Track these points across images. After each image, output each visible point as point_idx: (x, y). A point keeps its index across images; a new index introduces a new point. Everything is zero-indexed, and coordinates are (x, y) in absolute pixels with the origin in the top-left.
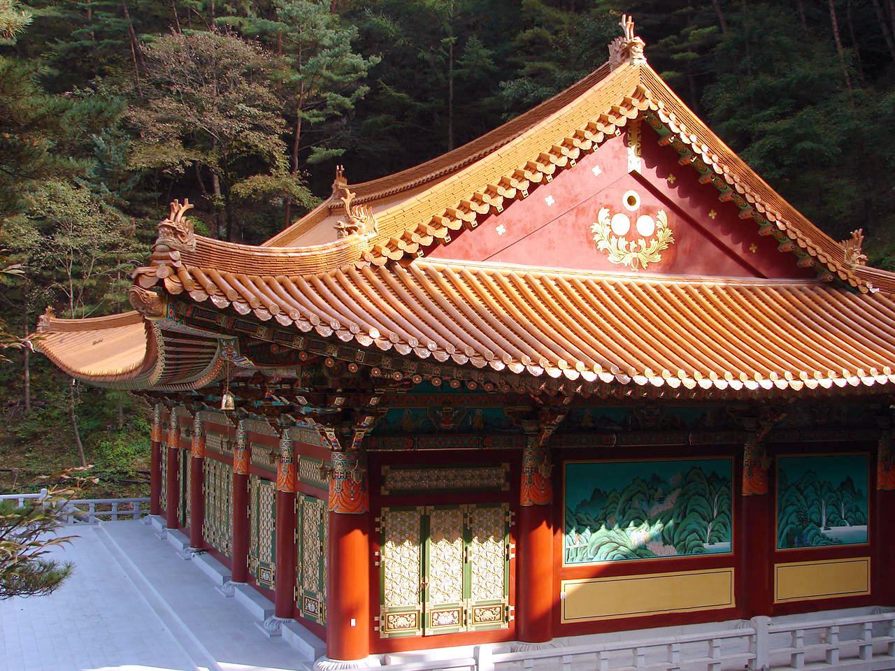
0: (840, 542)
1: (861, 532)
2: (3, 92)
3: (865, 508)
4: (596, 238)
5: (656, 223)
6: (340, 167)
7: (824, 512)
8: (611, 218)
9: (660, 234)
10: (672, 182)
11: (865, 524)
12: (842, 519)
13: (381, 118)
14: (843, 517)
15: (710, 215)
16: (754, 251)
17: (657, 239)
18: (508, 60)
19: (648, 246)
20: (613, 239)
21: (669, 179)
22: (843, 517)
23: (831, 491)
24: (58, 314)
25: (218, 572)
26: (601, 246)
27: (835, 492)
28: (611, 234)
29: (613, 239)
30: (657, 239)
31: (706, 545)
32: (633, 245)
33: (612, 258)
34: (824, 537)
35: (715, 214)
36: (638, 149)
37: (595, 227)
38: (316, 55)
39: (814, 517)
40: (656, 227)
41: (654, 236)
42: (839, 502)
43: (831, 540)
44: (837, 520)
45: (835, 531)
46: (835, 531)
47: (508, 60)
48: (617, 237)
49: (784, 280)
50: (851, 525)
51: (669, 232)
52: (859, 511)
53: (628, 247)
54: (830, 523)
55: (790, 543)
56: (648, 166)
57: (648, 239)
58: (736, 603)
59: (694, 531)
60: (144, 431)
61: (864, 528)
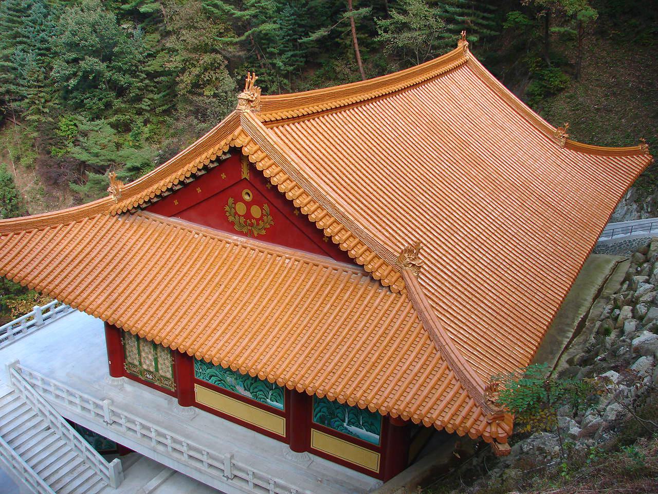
0: (358, 436)
4: (228, 214)
5: (262, 211)
7: (347, 415)
8: (235, 204)
9: (265, 218)
13: (217, 11)
17: (263, 221)
18: (496, 8)
19: (258, 224)
20: (237, 217)
24: (241, 7)
26: (231, 219)
28: (236, 213)
29: (237, 217)
30: (263, 221)
31: (268, 401)
32: (248, 221)
33: (236, 227)
34: (346, 429)
38: (542, 363)
39: (339, 415)
41: (261, 218)
43: (352, 433)
45: (353, 429)
46: (353, 429)
47: (496, 8)
48: (239, 216)
51: (270, 218)
52: (373, 425)
53: (245, 222)
55: (322, 419)
57: (258, 220)
59: (261, 391)
60: (559, 7)
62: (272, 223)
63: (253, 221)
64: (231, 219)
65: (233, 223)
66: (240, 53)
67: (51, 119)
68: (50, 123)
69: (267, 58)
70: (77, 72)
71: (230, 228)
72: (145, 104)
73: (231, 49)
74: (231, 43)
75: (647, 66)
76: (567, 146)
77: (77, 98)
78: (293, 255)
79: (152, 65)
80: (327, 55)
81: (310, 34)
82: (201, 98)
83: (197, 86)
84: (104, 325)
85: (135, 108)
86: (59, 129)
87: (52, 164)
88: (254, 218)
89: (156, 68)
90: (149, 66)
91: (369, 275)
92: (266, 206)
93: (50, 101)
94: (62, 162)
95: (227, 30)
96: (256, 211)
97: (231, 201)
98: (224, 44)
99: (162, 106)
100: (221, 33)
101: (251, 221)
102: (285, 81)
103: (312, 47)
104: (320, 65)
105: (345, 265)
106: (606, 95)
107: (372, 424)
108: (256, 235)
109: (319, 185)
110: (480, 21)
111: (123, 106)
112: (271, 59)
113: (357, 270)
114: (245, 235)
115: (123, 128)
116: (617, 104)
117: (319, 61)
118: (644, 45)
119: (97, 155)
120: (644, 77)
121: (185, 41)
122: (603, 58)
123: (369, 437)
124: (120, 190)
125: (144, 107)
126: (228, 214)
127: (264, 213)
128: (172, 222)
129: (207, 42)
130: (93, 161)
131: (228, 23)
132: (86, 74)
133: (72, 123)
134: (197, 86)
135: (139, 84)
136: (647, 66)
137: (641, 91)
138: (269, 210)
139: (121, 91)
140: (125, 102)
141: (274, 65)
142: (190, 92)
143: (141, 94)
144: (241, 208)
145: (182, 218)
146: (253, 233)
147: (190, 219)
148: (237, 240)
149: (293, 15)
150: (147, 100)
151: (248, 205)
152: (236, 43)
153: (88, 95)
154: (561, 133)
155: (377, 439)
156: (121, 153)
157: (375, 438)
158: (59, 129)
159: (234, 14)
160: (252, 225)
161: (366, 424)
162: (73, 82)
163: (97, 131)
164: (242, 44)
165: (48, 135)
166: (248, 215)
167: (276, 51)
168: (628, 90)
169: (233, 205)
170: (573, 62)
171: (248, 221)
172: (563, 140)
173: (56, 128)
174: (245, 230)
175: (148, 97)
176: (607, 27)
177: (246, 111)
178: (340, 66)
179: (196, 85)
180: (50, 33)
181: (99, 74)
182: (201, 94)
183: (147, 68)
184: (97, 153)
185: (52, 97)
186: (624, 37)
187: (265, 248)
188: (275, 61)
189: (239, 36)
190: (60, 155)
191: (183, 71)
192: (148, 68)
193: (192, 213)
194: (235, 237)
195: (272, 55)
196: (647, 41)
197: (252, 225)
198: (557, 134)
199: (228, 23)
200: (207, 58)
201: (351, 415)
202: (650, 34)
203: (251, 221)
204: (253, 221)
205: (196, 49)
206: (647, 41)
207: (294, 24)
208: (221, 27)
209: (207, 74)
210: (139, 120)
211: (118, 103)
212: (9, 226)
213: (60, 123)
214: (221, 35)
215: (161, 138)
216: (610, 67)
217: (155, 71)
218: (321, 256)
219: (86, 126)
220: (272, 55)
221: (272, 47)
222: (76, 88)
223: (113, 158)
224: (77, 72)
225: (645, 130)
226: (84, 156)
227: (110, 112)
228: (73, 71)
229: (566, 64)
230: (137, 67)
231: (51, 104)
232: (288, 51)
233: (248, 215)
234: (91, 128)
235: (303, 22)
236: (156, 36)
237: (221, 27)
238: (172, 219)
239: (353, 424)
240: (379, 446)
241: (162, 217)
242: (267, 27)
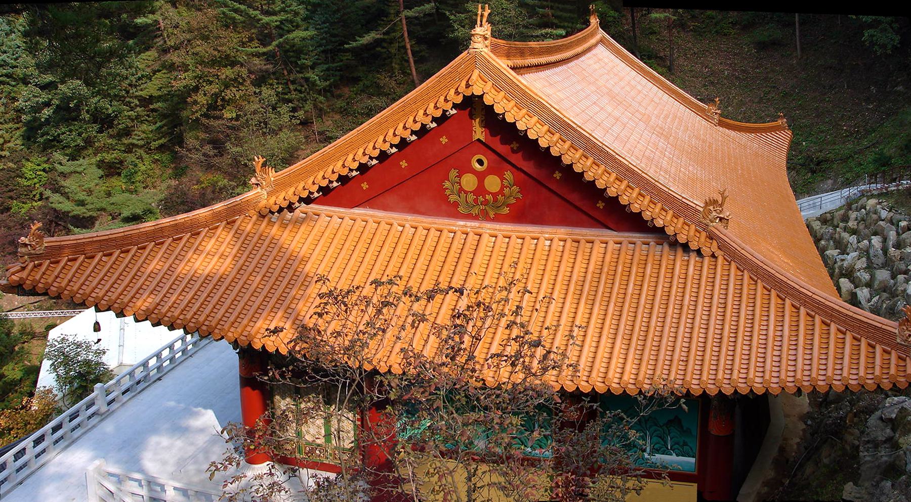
1: (688, 462)
2: (2, 150)
3: (695, 445)
4: (448, 192)
5: (502, 181)
6: (483, 8)
8: (460, 176)
9: (506, 191)
10: (515, 148)
11: (693, 457)
12: (668, 448)
14: (669, 448)
15: (555, 176)
16: (601, 207)
17: (503, 195)
20: (463, 195)
21: (512, 146)
22: (669, 448)
23: (657, 426)
25: (240, 375)
26: (453, 198)
27: (661, 427)
28: (461, 190)
29: (463, 195)
32: (481, 198)
33: (461, 209)
35: (560, 175)
36: (482, 121)
37: (447, 184)
40: (502, 185)
41: (501, 192)
42: (665, 435)
44: (662, 449)
45: (659, 457)
48: (466, 192)
49: (634, 235)
50: (677, 455)
51: (515, 189)
52: (687, 445)
53: (476, 201)
54: (655, 451)
56: (492, 135)
57: (495, 195)
58: (694, 483)
61: (693, 460)
62: (520, 196)
63: (488, 197)
64: (453, 198)
65: (456, 204)
66: (268, 66)
67: (11, 164)
68: (10, 170)
69: (298, 72)
70: (51, 100)
71: (452, 211)
72: (137, 138)
73: (256, 61)
74: (258, 55)
75: (735, 54)
76: (721, 124)
77: (48, 134)
78: (555, 233)
79: (145, 89)
80: (365, 68)
81: (358, 38)
82: (220, 122)
83: (215, 106)
84: (239, 383)
85: (125, 144)
86: (22, 176)
87: (12, 224)
88: (489, 193)
89: (152, 91)
90: (141, 90)
91: (674, 244)
92: (508, 175)
93: (9, 141)
94: (26, 220)
95: (251, 40)
96: (493, 183)
97: (453, 173)
98: (247, 55)
99: (160, 139)
100: (243, 43)
101: (484, 197)
102: (321, 98)
103: (347, 59)
104: (356, 80)
105: (630, 234)
106: (705, 85)
107: (685, 444)
108: (492, 216)
109: (591, 135)
110: (559, 13)
111: (110, 141)
112: (302, 73)
113: (647, 238)
114: (475, 218)
115: (111, 169)
116: (718, 93)
117: (355, 75)
118: (725, 35)
119: (82, 203)
120: (735, 64)
121: (197, 54)
122: (690, 49)
123: (679, 463)
124: (272, 179)
125: (135, 142)
126: (448, 192)
127: (506, 184)
128: (359, 214)
129: (228, 52)
130: (79, 211)
131: (252, 31)
132: (66, 99)
133: (39, 168)
134: (215, 106)
135: (131, 112)
136: (735, 54)
137: (737, 78)
138: (512, 177)
139: (104, 121)
140: (111, 137)
141: (307, 80)
142: (206, 116)
143: (132, 127)
144: (469, 182)
145: (372, 207)
146: (487, 213)
147: (385, 208)
148: (463, 226)
149: (324, 23)
150: (140, 133)
151: (481, 176)
152: (264, 54)
153: (63, 130)
154: (713, 109)
155: (692, 463)
156: (113, 200)
157: (688, 462)
158: (22, 176)
159: (261, 20)
160: (486, 203)
161: (676, 446)
162: (47, 112)
163: (80, 173)
164: (269, 57)
165: (7, 186)
166: (480, 190)
167: (309, 63)
168: (725, 79)
169: (457, 179)
170: (662, 54)
171: (481, 198)
172: (716, 117)
173: (18, 176)
174: (475, 211)
175: (140, 129)
176: (685, 19)
177: (484, 49)
178: (384, 79)
179: (212, 107)
180: (13, 55)
181: (82, 100)
182: (220, 117)
183: (140, 93)
184: (83, 201)
185: (12, 137)
186: (704, 28)
187: (500, 230)
188: (308, 75)
189: (265, 46)
190: (23, 211)
191: (196, 89)
192: (141, 92)
193: (390, 199)
194: (462, 223)
195: (303, 68)
196: (727, 31)
197: (486, 203)
198: (709, 111)
199: (252, 31)
200: (228, 72)
201: (655, 439)
202: (729, 23)
203: (484, 197)
204: (488, 197)
205: (214, 63)
206: (727, 31)
207: (326, 33)
208: (245, 35)
209: (228, 92)
210: (131, 158)
211: (103, 139)
212: (115, 239)
213: (24, 169)
214: (243, 44)
215: (156, 181)
216: (700, 58)
217: (151, 96)
218: (593, 229)
219: (68, 166)
220: (303, 68)
221: (304, 59)
222: (48, 121)
223: (104, 205)
224: (51, 100)
225: (755, 115)
226: (66, 206)
227: (90, 151)
228: (48, 98)
229: (657, 57)
230: (128, 92)
231: (11, 145)
232: (320, 64)
233: (480, 190)
234: (72, 169)
235: (335, 32)
236: (152, 54)
237: (245, 35)
238: (357, 211)
239: (657, 451)
240: (696, 473)
241: (342, 210)
242: (298, 35)
